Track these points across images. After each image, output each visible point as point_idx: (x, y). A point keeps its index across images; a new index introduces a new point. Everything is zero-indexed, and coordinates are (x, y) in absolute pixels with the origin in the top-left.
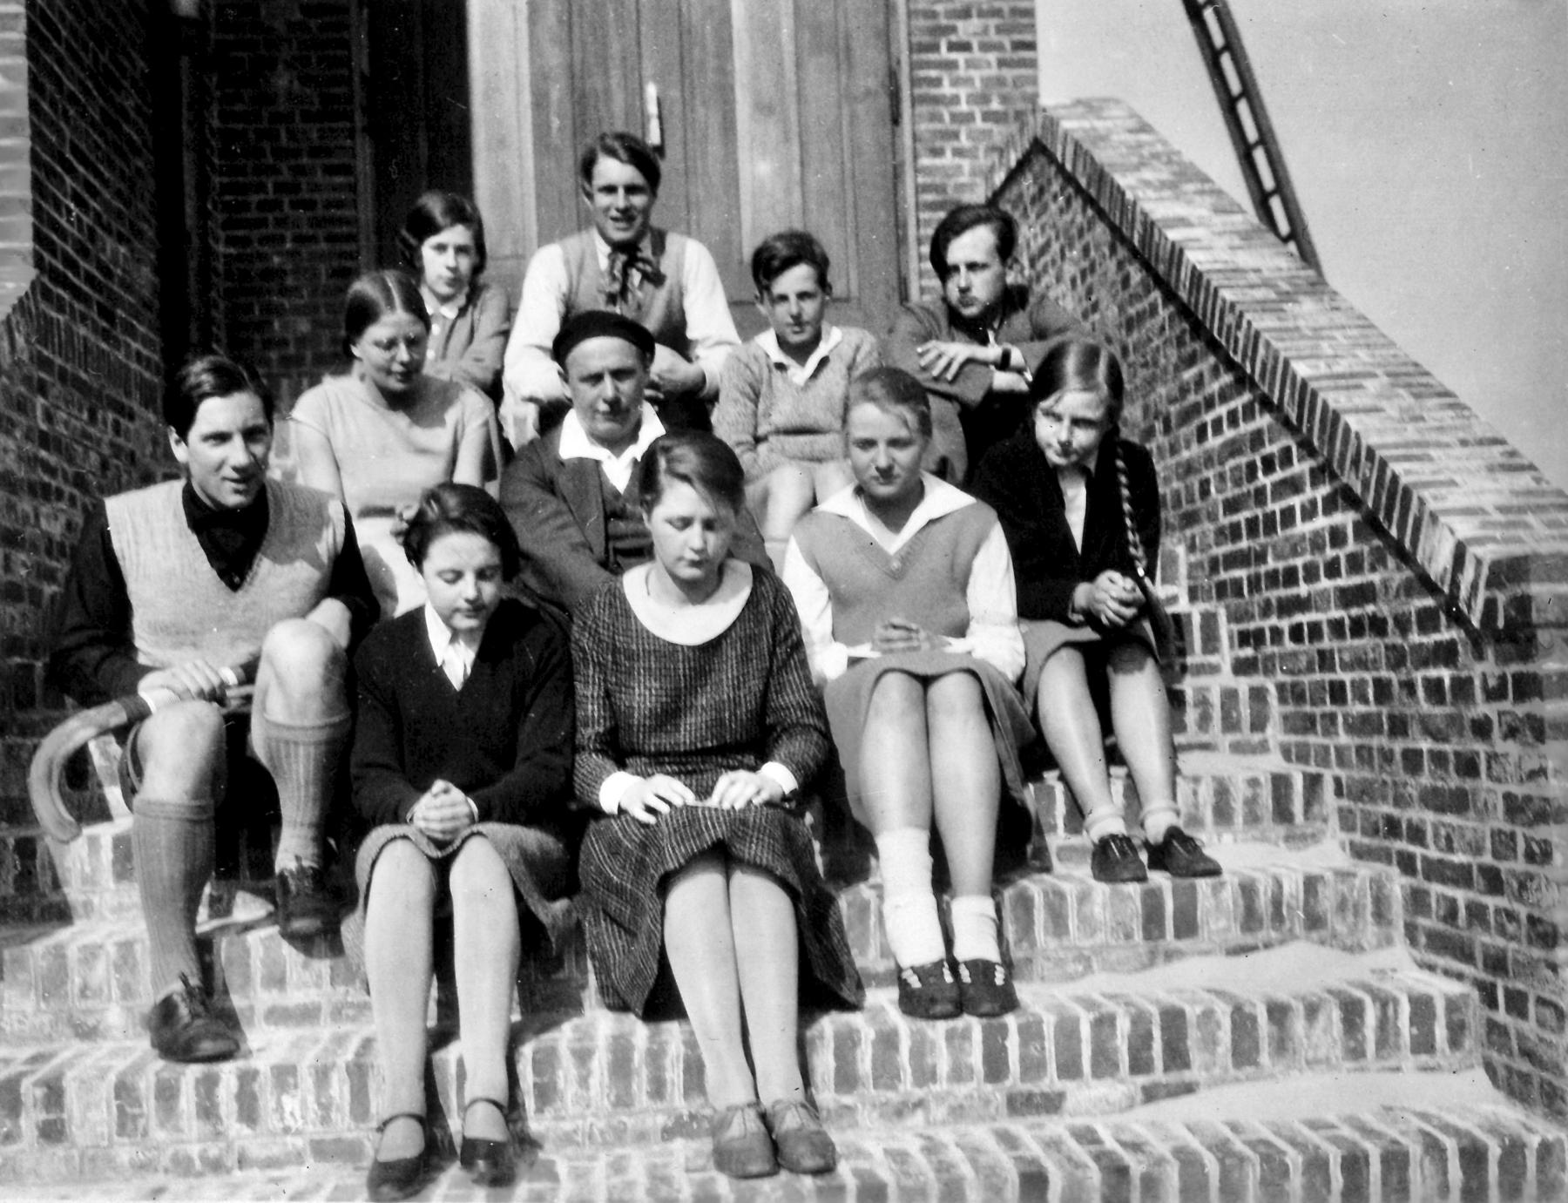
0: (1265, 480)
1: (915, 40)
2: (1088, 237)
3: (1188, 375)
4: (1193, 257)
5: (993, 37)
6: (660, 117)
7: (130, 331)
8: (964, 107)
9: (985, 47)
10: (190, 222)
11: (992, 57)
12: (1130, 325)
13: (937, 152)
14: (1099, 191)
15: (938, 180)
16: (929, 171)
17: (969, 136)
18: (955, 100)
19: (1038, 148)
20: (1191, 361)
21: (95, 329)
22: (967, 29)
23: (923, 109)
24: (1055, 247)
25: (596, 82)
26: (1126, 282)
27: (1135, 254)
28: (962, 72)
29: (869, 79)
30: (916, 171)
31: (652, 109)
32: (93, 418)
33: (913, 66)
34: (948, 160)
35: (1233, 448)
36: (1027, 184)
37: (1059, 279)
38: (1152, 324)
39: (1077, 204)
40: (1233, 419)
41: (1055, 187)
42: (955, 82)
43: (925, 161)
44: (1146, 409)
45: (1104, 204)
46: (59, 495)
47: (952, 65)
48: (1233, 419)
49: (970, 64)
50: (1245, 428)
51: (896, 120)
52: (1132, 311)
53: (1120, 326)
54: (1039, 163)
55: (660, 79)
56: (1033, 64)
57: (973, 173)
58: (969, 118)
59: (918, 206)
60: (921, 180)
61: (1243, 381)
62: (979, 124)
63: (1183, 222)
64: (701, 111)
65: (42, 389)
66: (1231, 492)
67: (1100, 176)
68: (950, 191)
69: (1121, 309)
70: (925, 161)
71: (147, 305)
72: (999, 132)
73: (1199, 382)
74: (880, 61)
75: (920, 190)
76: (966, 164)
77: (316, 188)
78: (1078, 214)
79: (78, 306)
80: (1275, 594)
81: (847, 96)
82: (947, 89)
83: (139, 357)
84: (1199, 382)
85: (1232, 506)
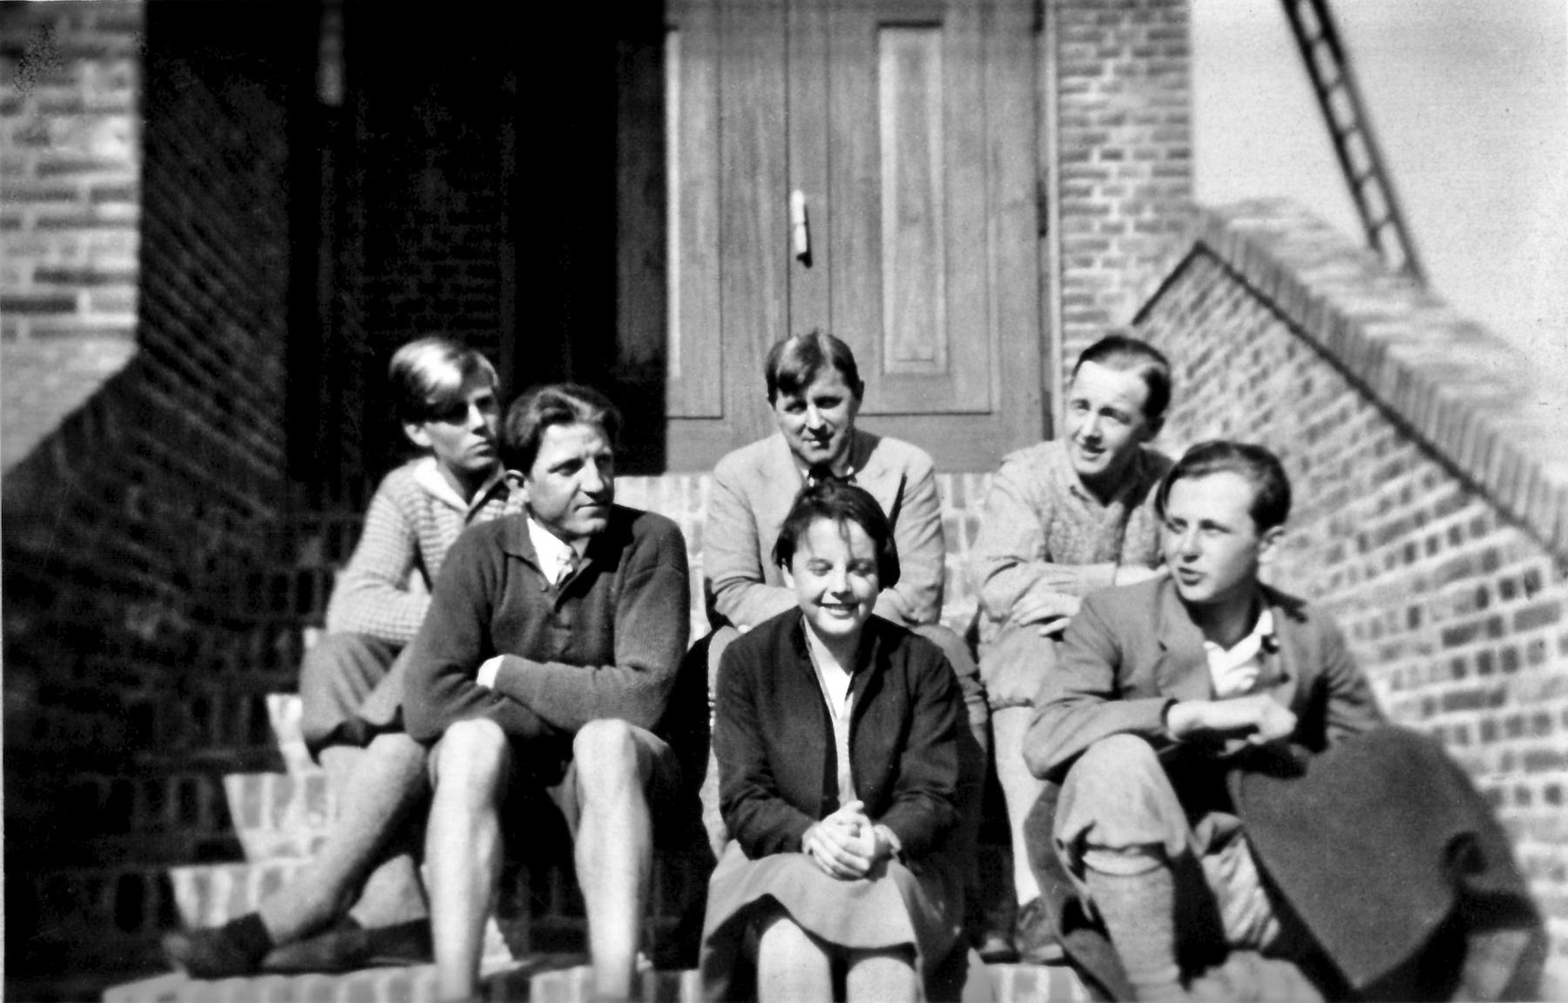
0: (1500, 607)
1: (1067, 148)
2: (1260, 342)
3: (1393, 487)
4: (1398, 352)
5: (1147, 144)
6: (807, 224)
7: (251, 423)
8: (1114, 217)
9: (1142, 156)
10: (324, 311)
11: (1146, 166)
12: (1313, 435)
13: (1087, 263)
14: (1276, 290)
15: (1085, 291)
16: (1078, 282)
17: (1122, 247)
18: (1104, 210)
19: (1200, 249)
20: (1394, 471)
21: (208, 418)
22: (1120, 137)
23: (1071, 220)
24: (1219, 355)
25: (745, 189)
26: (1307, 388)
27: (1324, 354)
28: (1113, 181)
29: (1016, 187)
30: (1064, 283)
31: (798, 217)
32: (200, 513)
33: (1062, 177)
34: (1096, 270)
35: (1460, 570)
36: (1185, 293)
37: (1223, 388)
38: (1343, 431)
39: (1249, 304)
40: (1455, 536)
41: (1220, 290)
42: (1110, 192)
43: (1073, 272)
44: (1334, 530)
45: (1282, 302)
46: (152, 593)
47: (1101, 175)
48: (1455, 536)
49: (1124, 173)
50: (1473, 547)
51: (1043, 232)
52: (1316, 419)
53: (1299, 437)
54: (1201, 264)
55: (807, 189)
56: (1186, 173)
57: (1125, 283)
58: (1118, 229)
59: (1064, 319)
60: (1068, 291)
61: (1469, 488)
62: (1130, 233)
63: (1377, 318)
64: (846, 220)
65: (138, 477)
66: (1453, 621)
67: (1278, 274)
68: (1098, 300)
69: (1302, 416)
70: (1073, 272)
71: (272, 399)
72: (1151, 243)
73: (1406, 496)
74: (1028, 178)
75: (1065, 301)
76: (1115, 275)
77: (456, 289)
78: (1250, 315)
79: (191, 391)
80: (1522, 745)
81: (992, 208)
82: (1097, 199)
83: (259, 452)
84: (1406, 496)
85: (1454, 638)
